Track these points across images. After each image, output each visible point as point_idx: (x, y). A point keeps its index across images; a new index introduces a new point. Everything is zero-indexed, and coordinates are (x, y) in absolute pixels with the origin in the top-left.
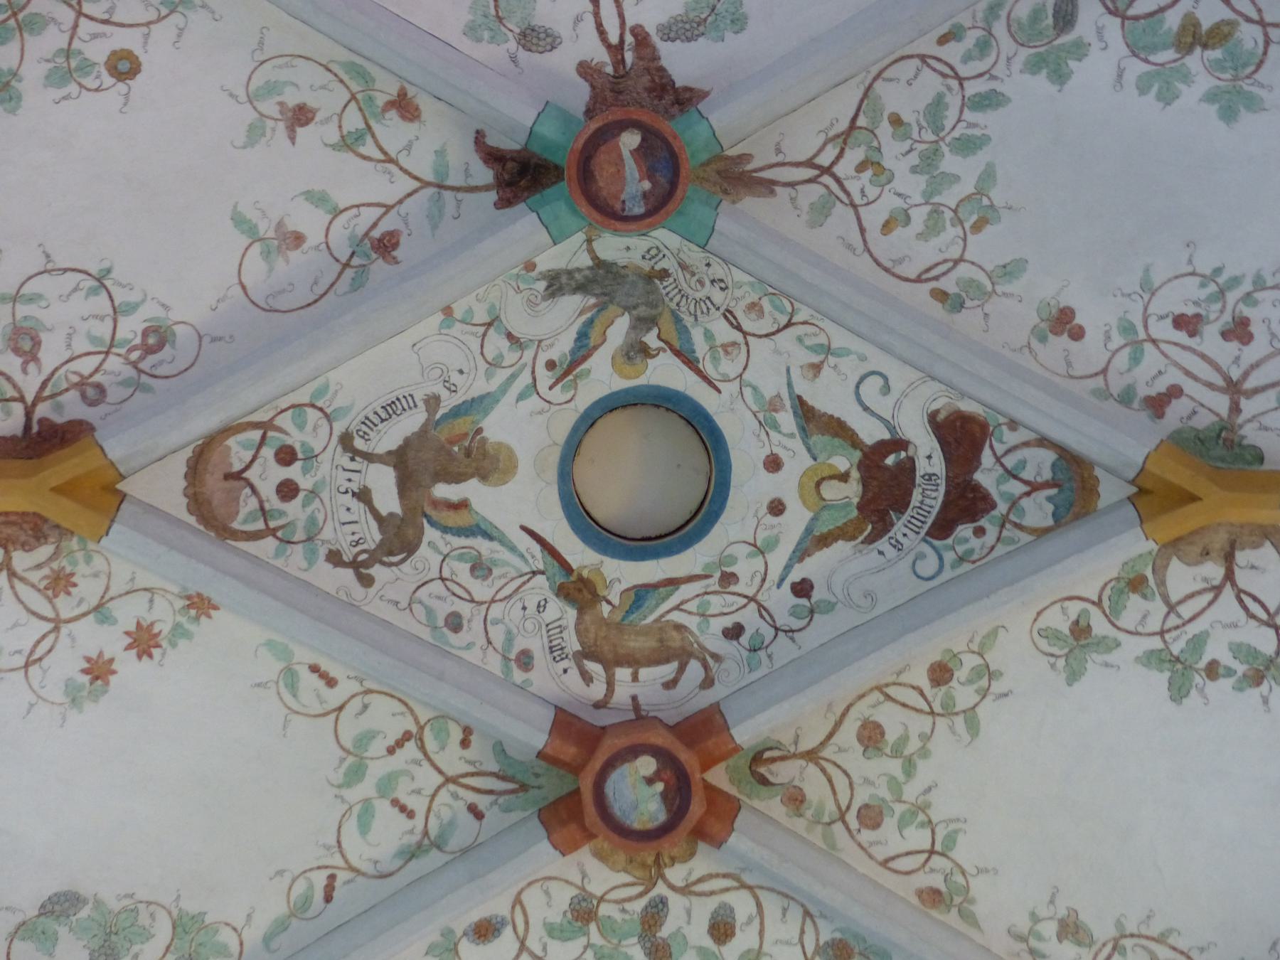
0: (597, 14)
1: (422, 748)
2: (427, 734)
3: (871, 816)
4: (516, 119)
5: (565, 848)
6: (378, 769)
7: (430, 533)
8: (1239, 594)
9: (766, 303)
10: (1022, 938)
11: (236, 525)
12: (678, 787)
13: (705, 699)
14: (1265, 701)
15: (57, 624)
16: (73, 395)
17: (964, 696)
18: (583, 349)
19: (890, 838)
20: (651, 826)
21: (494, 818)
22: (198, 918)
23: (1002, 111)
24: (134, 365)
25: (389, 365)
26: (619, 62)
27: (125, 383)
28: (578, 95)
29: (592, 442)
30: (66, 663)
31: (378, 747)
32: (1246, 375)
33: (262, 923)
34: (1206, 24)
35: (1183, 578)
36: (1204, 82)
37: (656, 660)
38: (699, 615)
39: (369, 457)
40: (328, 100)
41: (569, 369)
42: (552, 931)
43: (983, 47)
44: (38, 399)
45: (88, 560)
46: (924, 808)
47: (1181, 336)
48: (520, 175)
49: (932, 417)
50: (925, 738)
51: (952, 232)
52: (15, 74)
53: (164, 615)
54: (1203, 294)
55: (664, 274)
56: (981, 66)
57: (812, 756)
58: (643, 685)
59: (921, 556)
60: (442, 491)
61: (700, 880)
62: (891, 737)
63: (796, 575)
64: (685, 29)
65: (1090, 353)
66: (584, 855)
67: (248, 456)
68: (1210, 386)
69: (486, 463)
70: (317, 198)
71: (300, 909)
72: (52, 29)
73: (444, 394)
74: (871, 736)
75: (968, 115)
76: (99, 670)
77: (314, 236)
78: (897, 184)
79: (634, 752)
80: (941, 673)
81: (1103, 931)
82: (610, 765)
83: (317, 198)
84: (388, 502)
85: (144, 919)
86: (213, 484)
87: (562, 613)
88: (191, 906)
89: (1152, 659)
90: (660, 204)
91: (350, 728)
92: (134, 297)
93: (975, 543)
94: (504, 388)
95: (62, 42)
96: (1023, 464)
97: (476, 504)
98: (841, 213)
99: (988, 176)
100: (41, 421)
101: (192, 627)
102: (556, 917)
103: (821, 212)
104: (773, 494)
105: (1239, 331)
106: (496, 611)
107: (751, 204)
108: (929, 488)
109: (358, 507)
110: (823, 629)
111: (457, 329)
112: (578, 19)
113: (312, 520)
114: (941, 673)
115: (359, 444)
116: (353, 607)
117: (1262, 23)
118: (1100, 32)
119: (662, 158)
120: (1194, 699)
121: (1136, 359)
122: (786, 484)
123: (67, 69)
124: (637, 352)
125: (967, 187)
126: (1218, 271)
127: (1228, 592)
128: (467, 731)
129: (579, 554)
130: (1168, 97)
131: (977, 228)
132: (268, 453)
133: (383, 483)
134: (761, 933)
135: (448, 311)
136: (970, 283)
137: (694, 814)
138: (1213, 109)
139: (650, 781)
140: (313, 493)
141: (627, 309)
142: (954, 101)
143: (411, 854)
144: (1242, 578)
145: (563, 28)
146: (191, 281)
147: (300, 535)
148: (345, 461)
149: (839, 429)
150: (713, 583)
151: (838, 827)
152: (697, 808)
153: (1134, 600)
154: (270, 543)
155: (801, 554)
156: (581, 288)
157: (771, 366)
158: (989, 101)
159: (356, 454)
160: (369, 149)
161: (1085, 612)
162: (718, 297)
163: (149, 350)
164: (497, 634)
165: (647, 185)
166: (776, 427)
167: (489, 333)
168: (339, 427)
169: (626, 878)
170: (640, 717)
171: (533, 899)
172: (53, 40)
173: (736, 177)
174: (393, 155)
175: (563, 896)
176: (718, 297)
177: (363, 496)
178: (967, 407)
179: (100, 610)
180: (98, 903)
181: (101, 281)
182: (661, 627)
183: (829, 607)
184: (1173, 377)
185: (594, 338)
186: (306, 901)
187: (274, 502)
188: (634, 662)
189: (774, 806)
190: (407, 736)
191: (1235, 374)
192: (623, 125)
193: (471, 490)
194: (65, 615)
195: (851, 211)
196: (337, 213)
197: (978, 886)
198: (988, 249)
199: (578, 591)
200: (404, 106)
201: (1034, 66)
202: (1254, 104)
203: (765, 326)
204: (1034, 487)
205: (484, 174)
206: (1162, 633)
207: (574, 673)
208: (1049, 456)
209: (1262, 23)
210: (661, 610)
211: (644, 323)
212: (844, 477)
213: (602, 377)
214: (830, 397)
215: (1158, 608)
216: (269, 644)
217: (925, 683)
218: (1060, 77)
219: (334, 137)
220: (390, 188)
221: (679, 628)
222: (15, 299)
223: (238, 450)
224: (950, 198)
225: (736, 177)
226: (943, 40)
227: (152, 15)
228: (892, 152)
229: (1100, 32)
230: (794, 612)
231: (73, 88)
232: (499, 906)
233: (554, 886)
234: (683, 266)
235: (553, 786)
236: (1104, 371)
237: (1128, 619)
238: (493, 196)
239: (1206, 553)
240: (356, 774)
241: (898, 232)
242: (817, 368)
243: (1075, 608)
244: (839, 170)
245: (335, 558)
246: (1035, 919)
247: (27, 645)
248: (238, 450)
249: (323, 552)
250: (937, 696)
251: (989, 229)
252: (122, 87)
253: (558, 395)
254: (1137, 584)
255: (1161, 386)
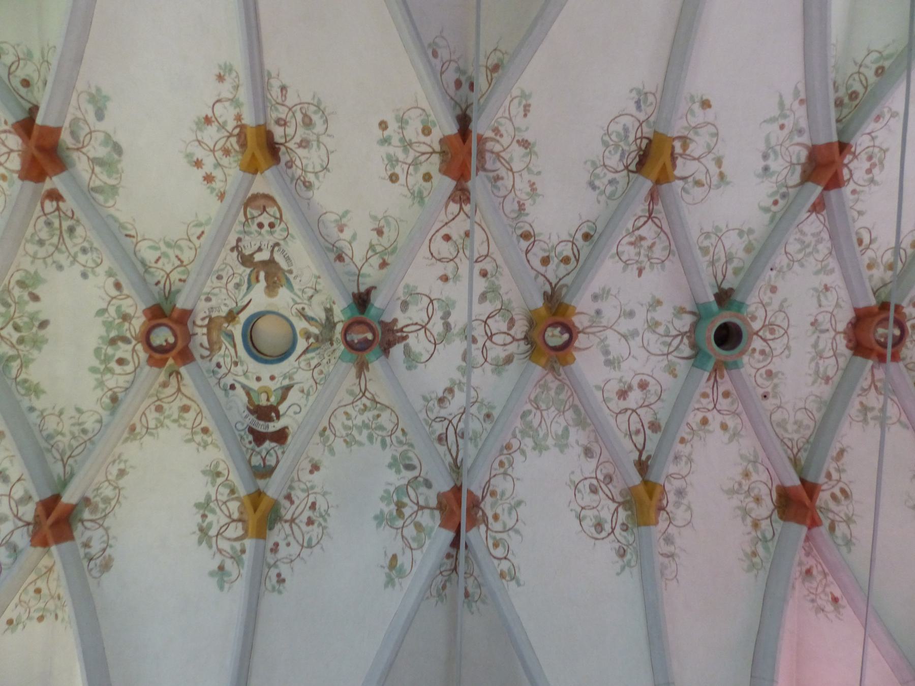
0: (412, 324)
1: (178, 267)
2: (182, 269)
3: (159, 409)
4: (378, 301)
5: (145, 312)
6: (171, 252)
7: (248, 270)
8: (228, 524)
9: (323, 376)
10: (119, 457)
11: (248, 209)
12: (164, 350)
13: (197, 356)
14: (194, 533)
15: (213, 151)
16: (288, 159)
17: (198, 438)
18: (309, 319)
19: (152, 415)
20: (152, 341)
21: (156, 289)
22: (116, 193)
23: (381, 449)
24: (299, 178)
25: (301, 259)
26: (398, 331)
27: (293, 175)
28: (387, 318)
29: (284, 321)
30: (200, 153)
31: (178, 252)
32: (296, 524)
33: (117, 214)
34: (404, 510)
35: (234, 506)
36: (386, 510)
37: (209, 341)
38: (224, 355)
39: (272, 252)
40: (385, 241)
41: (302, 314)
42: (118, 308)
43: (400, 442)
44: (287, 148)
45: (235, 161)
46: (162, 425)
47: (309, 504)
48: (362, 301)
49: (286, 428)
50: (185, 426)
51: (344, 433)
52: (390, 144)
53: (218, 185)
54: (322, 510)
55: (332, 344)
56: (394, 442)
57: (179, 390)
58: (201, 337)
59: (243, 424)
60: (262, 275)
61: (138, 355)
62: (186, 415)
63: (237, 385)
64: (407, 351)
65: (306, 476)
66: (143, 319)
67: (272, 213)
68: (294, 514)
69: (272, 288)
70: (354, 237)
71: (122, 226)
72: (404, 156)
73: (293, 275)
74: (185, 409)
75: (379, 438)
76: (198, 164)
77: (342, 236)
78: (359, 416)
79: (175, 336)
80: (205, 431)
81: (121, 483)
82: (171, 328)
83: (354, 237)
84: (258, 257)
85: (115, 176)
86: (262, 202)
87: (224, 312)
88: (121, 191)
89: (208, 498)
90: (350, 345)
91: (184, 243)
92: (321, 179)
93: (247, 441)
94: (295, 294)
95: (401, 159)
96: (271, 455)
97: (258, 285)
98: (351, 399)
99: (360, 444)
100: (279, 149)
101: (214, 194)
102: (123, 309)
103: (351, 393)
104: (263, 378)
105: (310, 522)
106: (224, 291)
107: (353, 371)
108: (263, 427)
109: (256, 247)
110: (220, 393)
111: (314, 280)
112: (411, 319)
113: (251, 233)
114: (205, 431)
115: (276, 249)
116: (223, 245)
117: (403, 527)
118: (403, 478)
119: (365, 346)
120: (195, 510)
121: (303, 490)
122: (266, 382)
123: (392, 161)
124: (308, 336)
125: (358, 438)
126: (329, 515)
127: (228, 520)
128: (184, 281)
129: (243, 317)
130: (382, 499)
131: (345, 441)
132: (272, 220)
133: (264, 256)
134: (120, 374)
135: (319, 277)
136: (328, 439)
137: (158, 355)
138: (378, 513)
139: (166, 341)
140: (260, 234)
141: (321, 333)
142: (384, 433)
143: (143, 263)
144: (233, 525)
145: (408, 314)
146: (327, 197)
147: (246, 229)
148: (271, 244)
149: (283, 398)
150: (235, 359)
151: (156, 398)
152: (157, 356)
153: (227, 491)
154: (243, 220)
155: (244, 387)
156: (327, 319)
157: (303, 377)
158: (384, 444)
159: (273, 247)
160: (370, 253)
161: (224, 476)
162: (325, 361)
163: (304, 183)
164: (216, 291)
165: (356, 341)
166: (284, 379)
167: (311, 292)
168: (282, 242)
169: (137, 331)
170: (189, 336)
171: (129, 301)
172: (401, 156)
173: (362, 367)
174: (370, 261)
175: (130, 311)
176: (325, 361)
177: (260, 249)
178: (290, 438)
179: (218, 165)
180: (119, 161)
181: (325, 169)
182: (220, 343)
183: (227, 395)
184: (297, 502)
185: (313, 322)
186: (126, 228)
187: (257, 221)
188: (209, 334)
189: (162, 378)
190: (182, 262)
191: (297, 521)
192: (374, 334)
193: (263, 283)
194: (216, 154)
195: (350, 401)
196: (350, 243)
197: (137, 443)
198: (339, 445)
199: (231, 317)
200: (384, 265)
201: (394, 458)
202: (379, 525)
203: (316, 375)
204: (264, 459)
205: (363, 289)
206: (217, 500)
207: (204, 315)
208: (273, 463)
209: (403, 527)
210: (226, 343)
211: (317, 338)
212: (268, 400)
213: (300, 325)
214: (294, 396)
215: (225, 498)
216: (210, 219)
217: (202, 425)
218: (390, 466)
219: (374, 243)
220: (358, 259)
221: (220, 348)
222: (318, 141)
223: (272, 210)
224: (355, 433)
225: (362, 367)
226: (403, 430)
227: (410, 187)
228: (369, 415)
229: (403, 478)
230: (225, 385)
231: (386, 162)
232: (126, 291)
233: (133, 308)
234: (334, 350)
235: (167, 308)
236: (299, 480)
237: (221, 489)
238: (356, 291)
239: (241, 513)
240: (168, 245)
241: (344, 417)
242: (302, 391)
243: (226, 473)
244: (364, 399)
245: (239, 240)
246: (126, 461)
247: (205, 141)
248: (272, 210)
249: (241, 236)
250: (198, 429)
251: (344, 445)
252: (387, 177)
253: (294, 311)
254: (233, 491)
255: (294, 498)
